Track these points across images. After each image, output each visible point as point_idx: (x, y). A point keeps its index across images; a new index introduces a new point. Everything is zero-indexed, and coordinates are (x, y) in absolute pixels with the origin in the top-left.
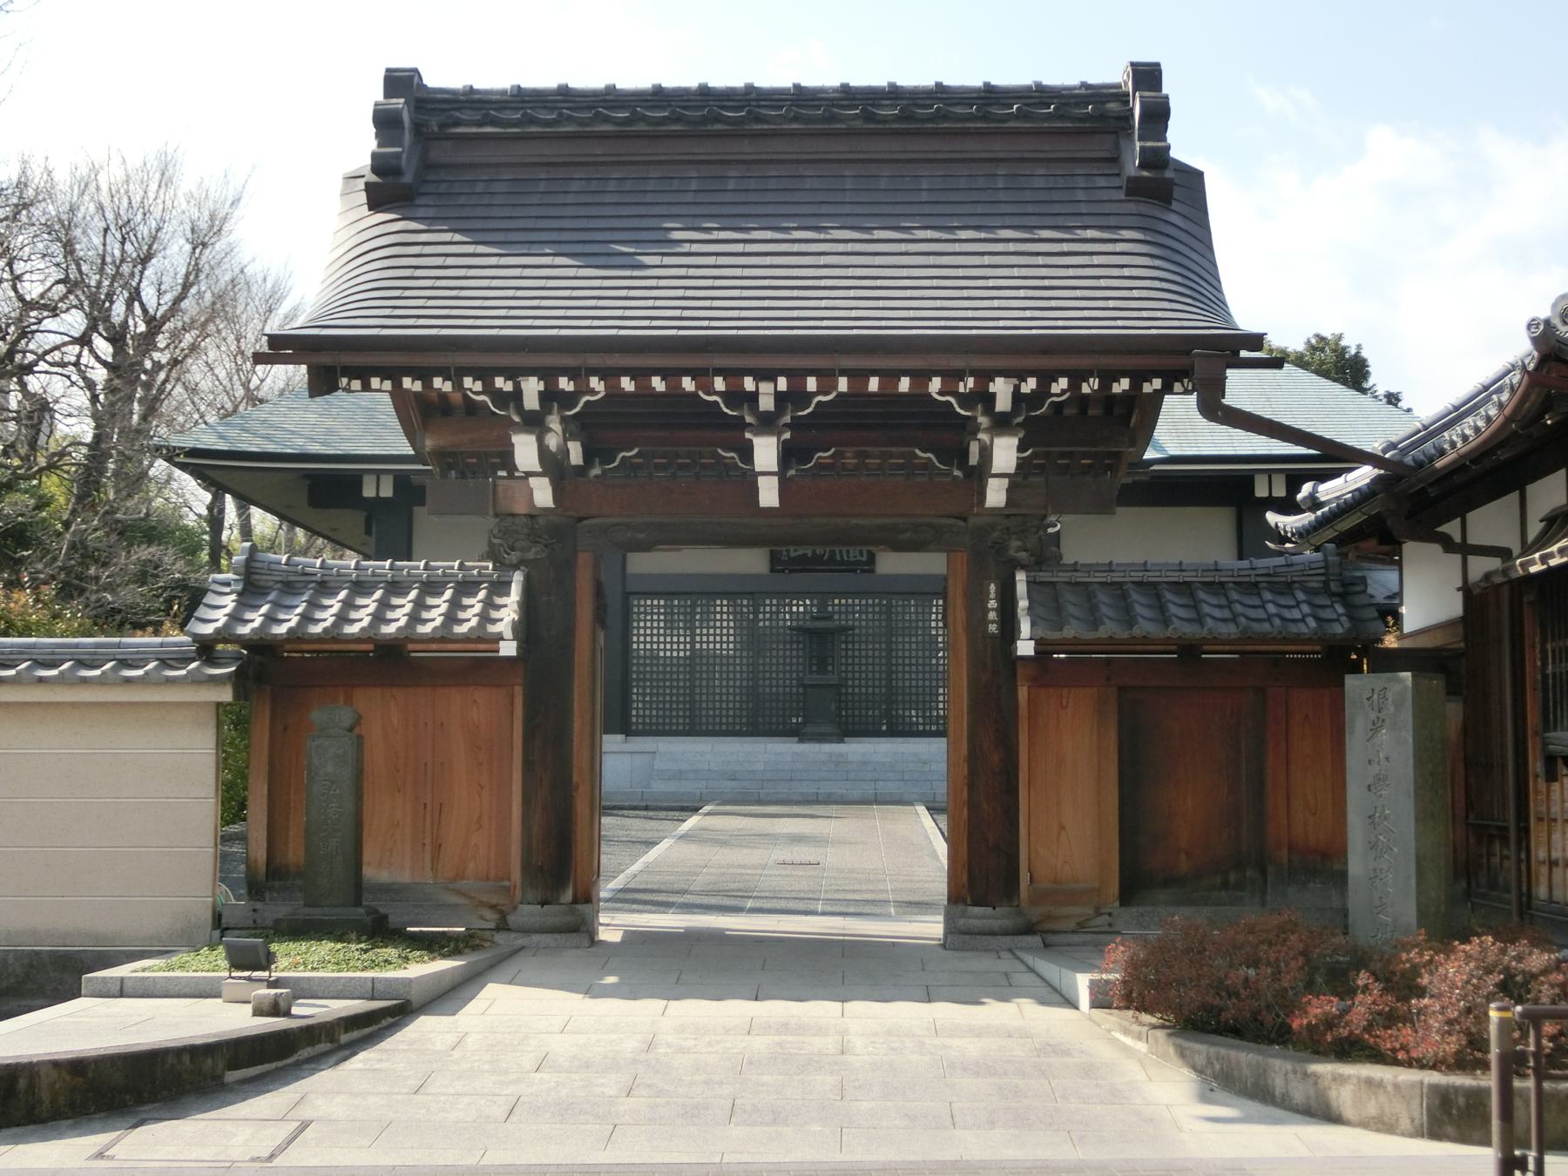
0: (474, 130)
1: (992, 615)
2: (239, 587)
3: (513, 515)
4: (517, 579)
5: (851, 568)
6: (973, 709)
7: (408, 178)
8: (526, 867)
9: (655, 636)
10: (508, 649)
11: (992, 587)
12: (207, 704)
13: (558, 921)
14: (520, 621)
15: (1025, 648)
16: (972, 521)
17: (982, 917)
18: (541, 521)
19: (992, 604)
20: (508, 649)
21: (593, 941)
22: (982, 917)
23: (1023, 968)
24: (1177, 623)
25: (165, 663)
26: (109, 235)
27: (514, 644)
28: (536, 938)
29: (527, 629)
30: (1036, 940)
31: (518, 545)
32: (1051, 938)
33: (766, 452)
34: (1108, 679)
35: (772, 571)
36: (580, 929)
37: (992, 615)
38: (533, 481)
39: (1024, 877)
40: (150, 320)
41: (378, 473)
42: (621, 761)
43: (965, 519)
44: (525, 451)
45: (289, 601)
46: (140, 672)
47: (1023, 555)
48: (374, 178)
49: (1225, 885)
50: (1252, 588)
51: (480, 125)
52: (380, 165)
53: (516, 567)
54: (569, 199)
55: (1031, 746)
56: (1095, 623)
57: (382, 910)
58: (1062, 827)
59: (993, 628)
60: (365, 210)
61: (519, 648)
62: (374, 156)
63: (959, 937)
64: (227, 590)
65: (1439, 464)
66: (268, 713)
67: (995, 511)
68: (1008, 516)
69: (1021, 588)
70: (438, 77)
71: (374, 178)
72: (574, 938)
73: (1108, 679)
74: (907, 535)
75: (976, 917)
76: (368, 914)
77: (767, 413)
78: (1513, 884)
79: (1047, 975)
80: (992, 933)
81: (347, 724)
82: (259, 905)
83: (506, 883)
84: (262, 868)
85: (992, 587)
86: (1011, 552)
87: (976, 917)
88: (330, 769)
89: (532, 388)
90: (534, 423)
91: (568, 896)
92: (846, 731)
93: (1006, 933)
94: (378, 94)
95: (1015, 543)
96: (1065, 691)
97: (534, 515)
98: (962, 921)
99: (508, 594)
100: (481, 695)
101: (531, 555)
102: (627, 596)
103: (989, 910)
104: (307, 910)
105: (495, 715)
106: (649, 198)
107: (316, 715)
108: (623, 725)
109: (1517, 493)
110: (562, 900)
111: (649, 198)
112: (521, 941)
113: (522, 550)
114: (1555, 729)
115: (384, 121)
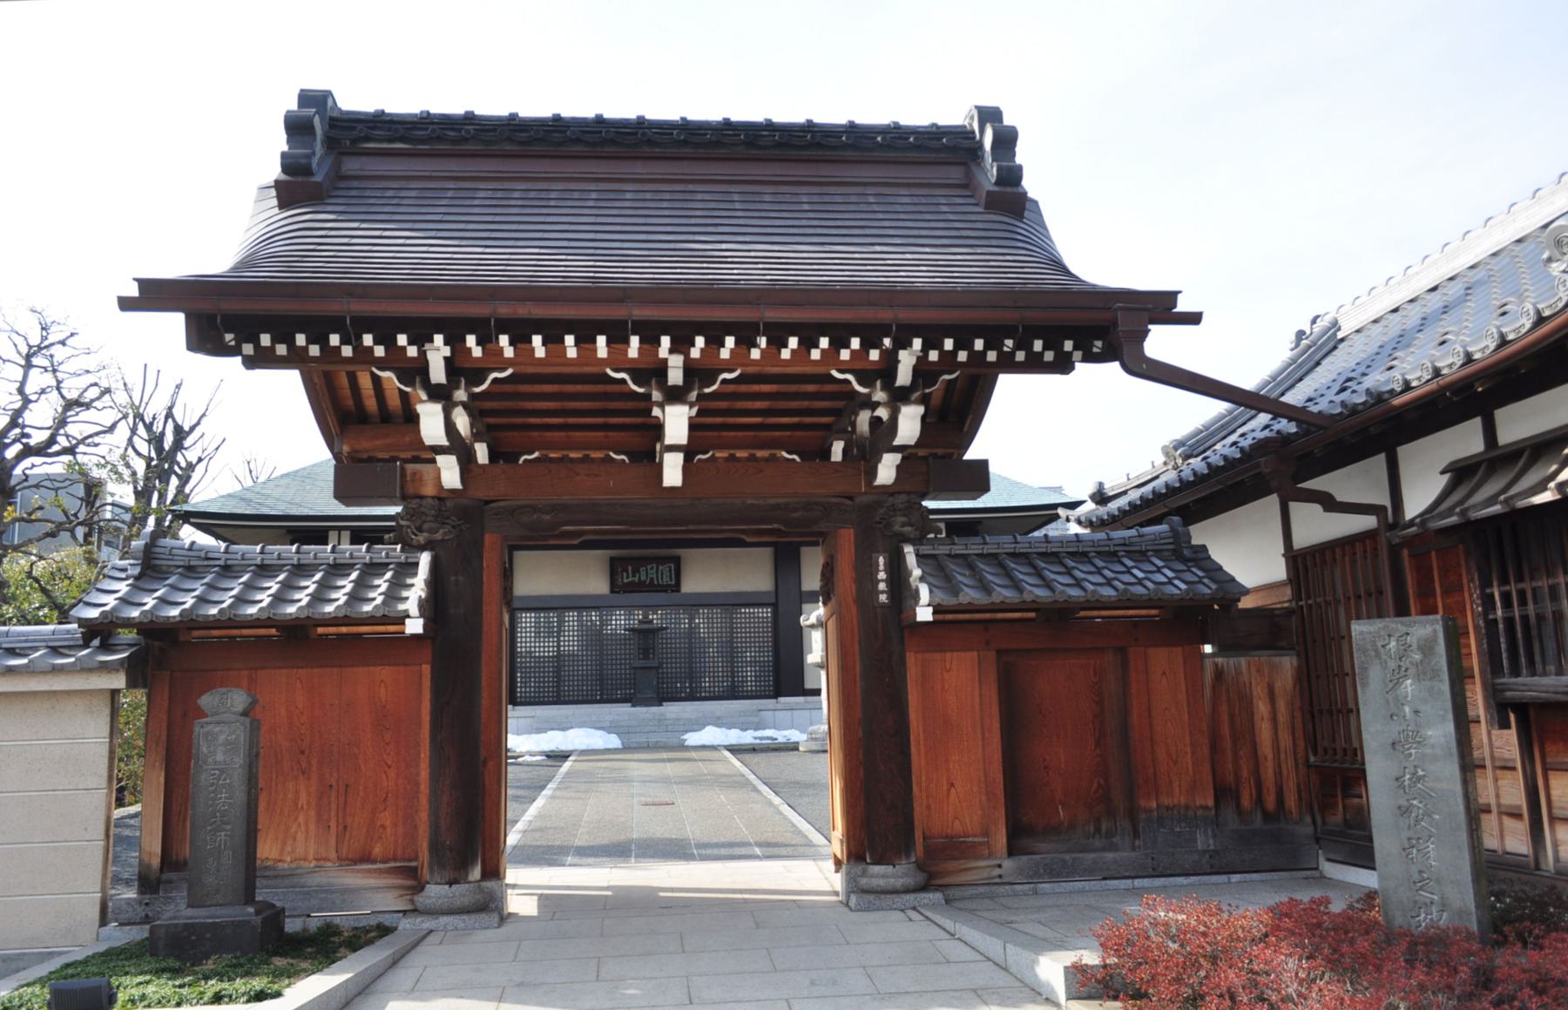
0: (385, 145)
1: (882, 586)
2: (137, 571)
3: (422, 497)
4: (425, 559)
5: (663, 589)
7: (318, 178)
8: (435, 847)
9: (531, 637)
10: (415, 626)
11: (881, 560)
12: (101, 690)
13: (466, 901)
14: (427, 600)
15: (924, 614)
16: (858, 500)
17: (884, 876)
18: (448, 504)
19: (882, 575)
20: (415, 626)
21: (504, 918)
22: (884, 876)
23: (970, 955)
25: (55, 651)
27: (421, 621)
28: (444, 920)
29: (433, 607)
30: (937, 897)
32: (951, 892)
33: (676, 422)
34: (987, 643)
35: (612, 591)
36: (489, 906)
37: (882, 586)
38: (440, 459)
39: (918, 834)
40: (178, 430)
41: (340, 529)
42: (526, 738)
43: (851, 498)
44: (431, 423)
45: (188, 585)
46: (24, 661)
47: (908, 529)
48: (284, 177)
50: (1111, 556)
52: (290, 165)
54: (476, 202)
56: (955, 591)
57: (278, 904)
59: (883, 598)
60: (276, 210)
61: (425, 626)
62: (284, 155)
63: (861, 895)
64: (123, 575)
65: (1397, 401)
67: (884, 488)
69: (911, 560)
70: (353, 99)
71: (284, 177)
72: (483, 918)
73: (987, 643)
75: (877, 876)
76: (257, 913)
77: (675, 387)
80: (895, 892)
81: (240, 708)
83: (413, 864)
84: (156, 862)
85: (881, 560)
86: (897, 528)
87: (877, 876)
88: (220, 757)
89: (438, 352)
90: (439, 394)
91: (476, 873)
92: (660, 699)
93: (907, 891)
94: (293, 105)
96: (948, 655)
97: (444, 496)
99: (416, 574)
100: (384, 673)
101: (438, 536)
103: (890, 868)
104: (190, 912)
105: (411, 691)
106: (552, 203)
107: (206, 701)
108: (514, 701)
109: (1382, 457)
110: (471, 878)
111: (552, 203)
112: (428, 923)
113: (430, 531)
114: (1516, 672)
115: (296, 127)
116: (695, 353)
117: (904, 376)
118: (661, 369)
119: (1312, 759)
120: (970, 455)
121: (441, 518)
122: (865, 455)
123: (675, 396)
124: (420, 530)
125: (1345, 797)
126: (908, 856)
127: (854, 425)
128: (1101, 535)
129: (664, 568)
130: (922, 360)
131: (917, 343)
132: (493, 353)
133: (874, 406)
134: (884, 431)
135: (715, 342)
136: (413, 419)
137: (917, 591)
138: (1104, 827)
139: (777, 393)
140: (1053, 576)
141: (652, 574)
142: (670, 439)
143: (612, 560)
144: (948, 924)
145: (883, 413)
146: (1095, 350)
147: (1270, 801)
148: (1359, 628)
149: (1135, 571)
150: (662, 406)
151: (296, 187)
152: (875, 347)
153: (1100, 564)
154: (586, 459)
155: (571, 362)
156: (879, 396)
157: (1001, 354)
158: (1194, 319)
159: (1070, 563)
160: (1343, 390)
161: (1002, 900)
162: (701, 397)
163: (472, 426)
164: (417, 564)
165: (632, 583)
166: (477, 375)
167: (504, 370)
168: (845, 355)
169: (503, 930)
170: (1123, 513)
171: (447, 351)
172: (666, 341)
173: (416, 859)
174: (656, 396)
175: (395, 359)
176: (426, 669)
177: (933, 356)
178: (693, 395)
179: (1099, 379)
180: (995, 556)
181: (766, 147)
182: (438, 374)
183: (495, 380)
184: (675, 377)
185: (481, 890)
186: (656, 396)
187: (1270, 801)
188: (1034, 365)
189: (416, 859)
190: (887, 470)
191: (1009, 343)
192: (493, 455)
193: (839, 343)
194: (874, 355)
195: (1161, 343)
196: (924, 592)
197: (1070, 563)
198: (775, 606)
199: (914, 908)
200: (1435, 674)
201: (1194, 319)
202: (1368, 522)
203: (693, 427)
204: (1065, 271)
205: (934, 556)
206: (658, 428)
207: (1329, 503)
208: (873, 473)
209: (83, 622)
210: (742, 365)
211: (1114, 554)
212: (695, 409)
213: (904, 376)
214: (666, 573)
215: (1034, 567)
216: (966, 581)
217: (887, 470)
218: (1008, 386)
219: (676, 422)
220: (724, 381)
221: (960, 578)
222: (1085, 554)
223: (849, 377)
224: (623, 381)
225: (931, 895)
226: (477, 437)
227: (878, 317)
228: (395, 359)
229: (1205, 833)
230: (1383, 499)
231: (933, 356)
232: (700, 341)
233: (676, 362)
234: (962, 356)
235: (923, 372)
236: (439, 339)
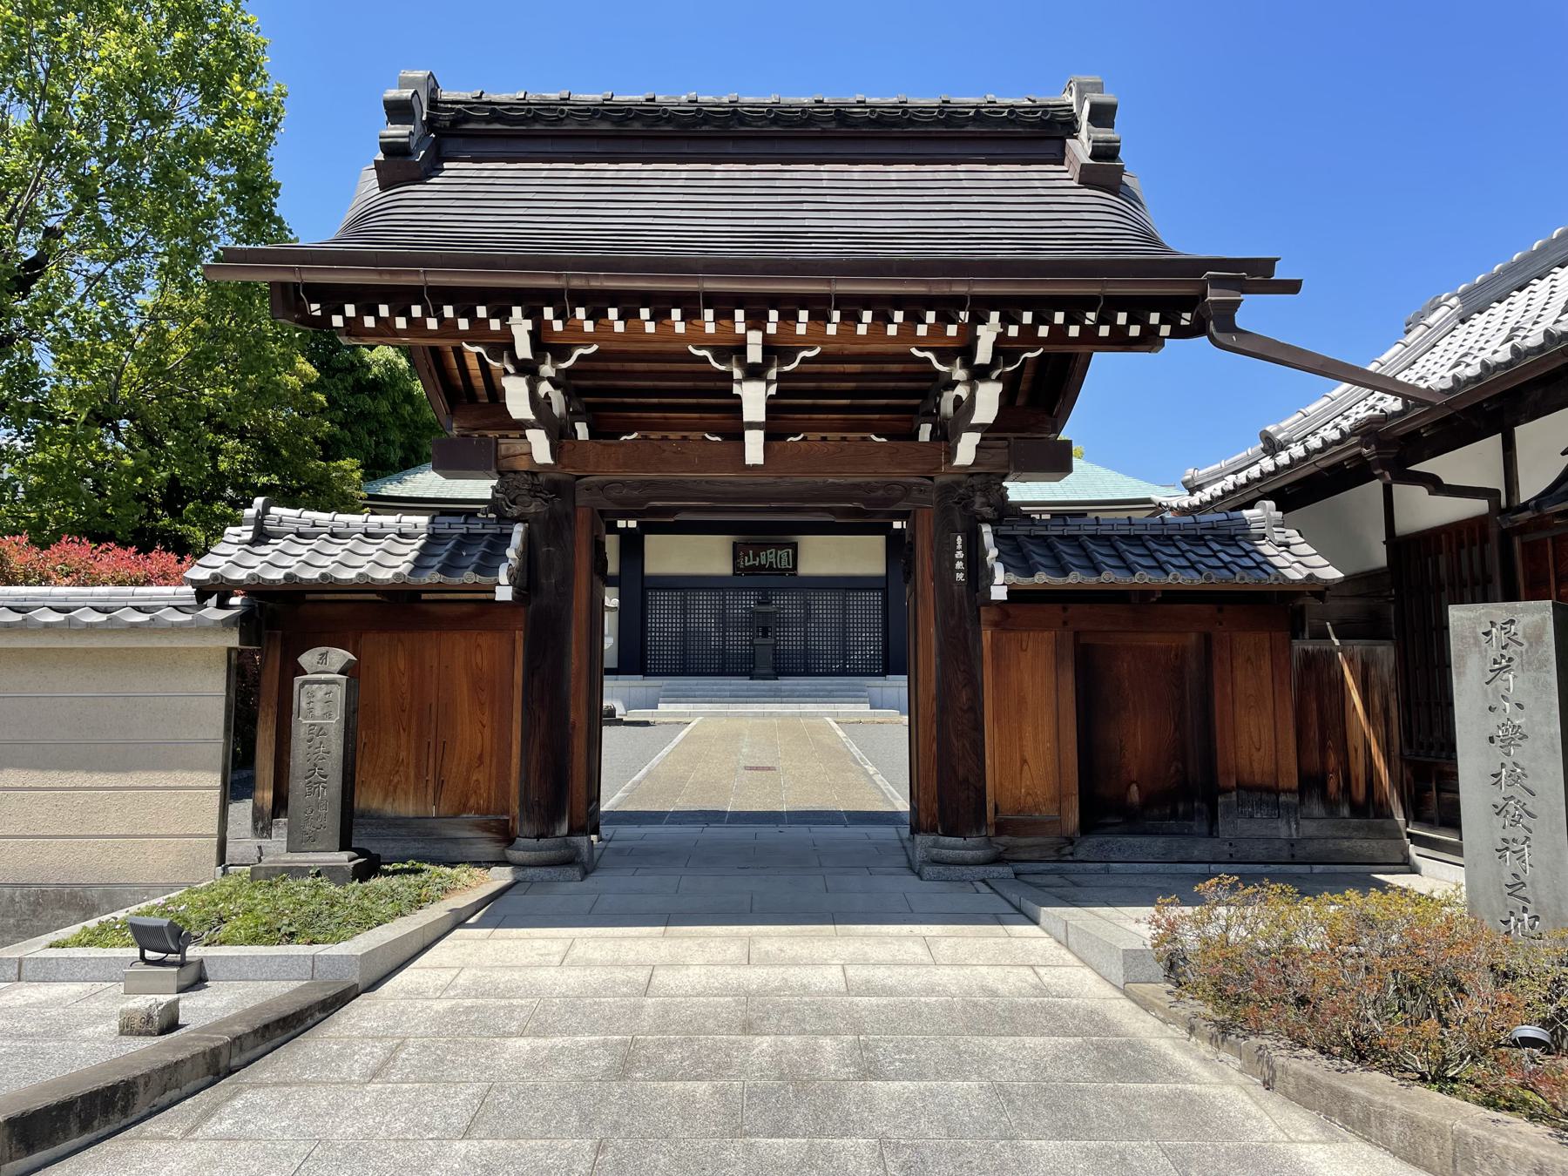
1: (959, 565)
3: (516, 472)
4: (518, 531)
6: (942, 653)
8: (525, 803)
11: (959, 539)
13: (552, 854)
18: (541, 478)
19: (959, 555)
20: (504, 593)
24: (1173, 572)
26: (880, 797)
29: (526, 580)
31: (519, 500)
33: (754, 399)
34: (1065, 623)
37: (959, 565)
38: (529, 433)
39: (990, 806)
43: (931, 479)
44: (517, 398)
49: (1174, 815)
51: (489, 122)
53: (517, 520)
55: (996, 685)
58: (1024, 761)
59: (960, 576)
66: (278, 654)
68: (972, 475)
74: (881, 492)
77: (754, 365)
78: (456, 581)
79: (1008, 896)
82: (264, 842)
85: (959, 539)
86: (976, 507)
89: (521, 328)
90: (528, 370)
95: (979, 499)
96: (1025, 635)
97: (535, 471)
98: (935, 851)
102: (644, 591)
105: (506, 656)
107: (307, 659)
116: (771, 329)
117: (984, 355)
118: (741, 349)
119: (1406, 752)
120: (1062, 436)
121: (534, 491)
122: (946, 435)
123: (754, 373)
124: (514, 502)
125: (1439, 791)
126: (978, 830)
127: (938, 406)
128: (1190, 519)
129: (783, 553)
130: (1002, 338)
131: (995, 316)
132: (574, 329)
133: (952, 385)
134: (965, 407)
135: (789, 317)
136: (496, 396)
137: (993, 569)
138: (1181, 809)
139: (862, 373)
140: (1133, 558)
141: (772, 558)
142: (748, 416)
143: (735, 545)
144: (1014, 898)
145: (962, 391)
146: (1183, 323)
147: (1360, 793)
148: (1458, 615)
149: (1221, 555)
150: (739, 382)
151: (398, 167)
152: (953, 323)
153: (1185, 547)
154: (665, 438)
155: (650, 338)
156: (960, 374)
157: (1084, 329)
158: (1292, 287)
159: (1153, 546)
160: (1457, 365)
161: (1075, 878)
162: (781, 377)
163: (568, 406)
164: (510, 535)
165: (752, 567)
166: (561, 353)
167: (589, 346)
168: (922, 330)
169: (590, 882)
170: (1214, 499)
171: (528, 324)
172: (739, 314)
173: (507, 813)
174: (737, 373)
175: (479, 331)
176: (519, 635)
177: (1013, 331)
178: (772, 374)
179: (1188, 357)
180: (1076, 538)
181: (927, 124)
182: (524, 350)
183: (581, 357)
184: (755, 355)
185: (567, 846)
186: (737, 373)
187: (1360, 793)
188: (1120, 341)
189: (507, 813)
190: (966, 450)
191: (1091, 316)
192: (593, 434)
193: (915, 318)
194: (952, 330)
195: (1256, 313)
196: (999, 575)
197: (1153, 546)
198: (885, 592)
199: (983, 881)
200: (1542, 665)
201: (1292, 287)
202: (1480, 506)
203: (771, 408)
204: (1156, 242)
205: (1013, 537)
206: (737, 408)
207: (1435, 485)
208: (952, 453)
209: (193, 582)
210: (821, 343)
211: (1201, 538)
212: (773, 390)
213: (984, 355)
214: (785, 558)
215: (1116, 549)
216: (1042, 560)
217: (966, 450)
218: (1103, 364)
219: (754, 399)
220: (804, 360)
221: (1038, 559)
222: (1170, 537)
223: (929, 355)
224: (704, 360)
225: (1000, 869)
226: (574, 415)
227: (950, 287)
228: (479, 331)
229: (1288, 823)
230: (1496, 482)
231: (1013, 331)
232: (774, 315)
233: (755, 338)
234: (1043, 331)
235: (1002, 348)
236: (517, 311)
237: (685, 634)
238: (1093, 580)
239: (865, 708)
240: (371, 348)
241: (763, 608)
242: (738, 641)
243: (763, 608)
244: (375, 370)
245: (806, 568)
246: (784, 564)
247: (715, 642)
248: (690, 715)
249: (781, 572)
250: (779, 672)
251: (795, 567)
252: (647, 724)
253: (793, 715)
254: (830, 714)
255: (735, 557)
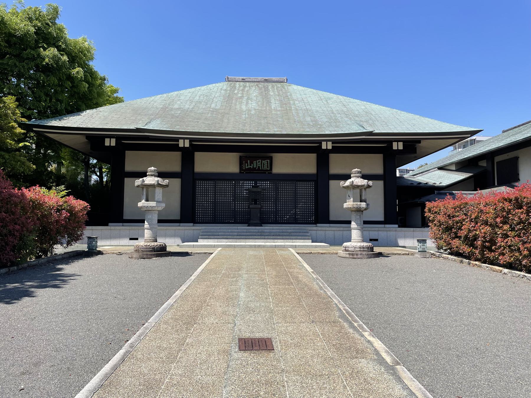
129: (265, 162)
141: (259, 164)
237: (215, 203)
238: (156, 244)
239: (309, 243)
240: (45, 49)
241: (255, 190)
242: (242, 206)
243: (255, 190)
244: (47, 60)
245: (277, 170)
246: (265, 168)
247: (33, 30)
248: (214, 246)
249: (264, 172)
250: (262, 222)
251: (271, 169)
252: (186, 254)
253: (271, 247)
254: (292, 246)
255: (241, 164)
